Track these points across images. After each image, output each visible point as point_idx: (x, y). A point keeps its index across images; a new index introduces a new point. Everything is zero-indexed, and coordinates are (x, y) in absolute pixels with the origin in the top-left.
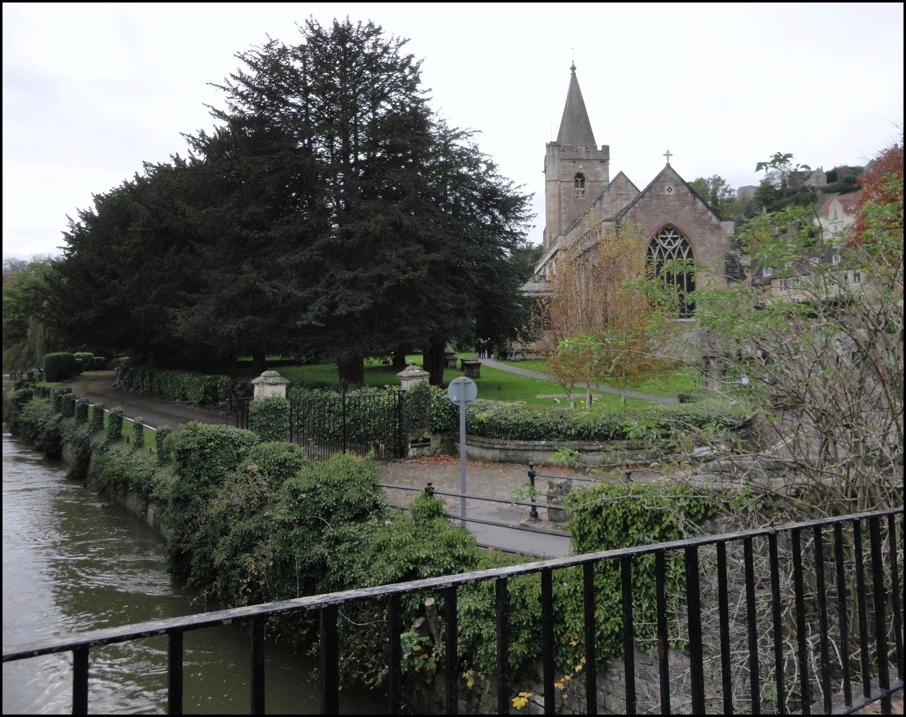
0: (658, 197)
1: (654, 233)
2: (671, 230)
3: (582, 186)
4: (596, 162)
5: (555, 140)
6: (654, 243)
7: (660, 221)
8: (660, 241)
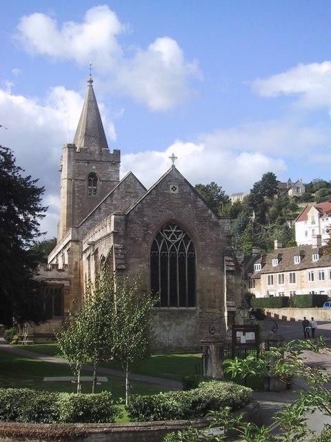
6: (159, 236)
7: (164, 217)
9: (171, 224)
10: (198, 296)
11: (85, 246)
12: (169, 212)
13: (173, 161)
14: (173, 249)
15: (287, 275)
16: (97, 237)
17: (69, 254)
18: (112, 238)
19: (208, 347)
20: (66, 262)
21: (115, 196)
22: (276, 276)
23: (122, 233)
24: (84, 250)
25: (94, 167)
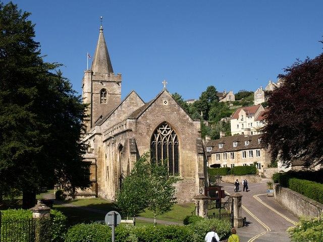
6: (156, 132)
15: (254, 151)
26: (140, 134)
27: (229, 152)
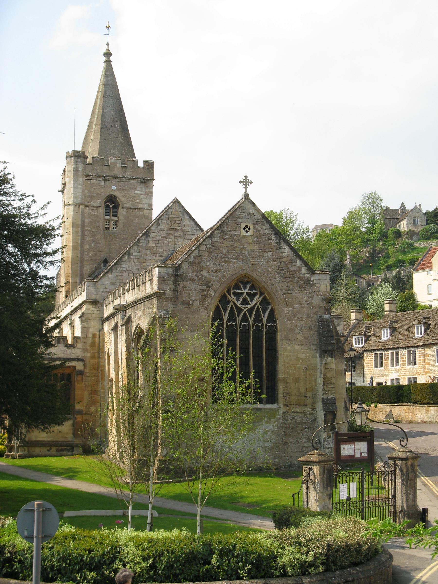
0: (231, 237)
1: (225, 285)
2: (247, 283)
3: (115, 215)
4: (135, 183)
5: (79, 148)
6: (224, 300)
7: (234, 269)
8: (233, 298)
9: (243, 281)
10: (281, 387)
11: (108, 311)
12: (239, 264)
13: (246, 188)
14: (245, 319)
15: (403, 353)
16: (129, 298)
17: (82, 321)
18: (154, 301)
19: (311, 469)
20: (78, 333)
21: (153, 235)
22: (387, 355)
23: (169, 293)
24: (106, 315)
25: (114, 187)
26: (186, 303)
27: (403, 348)
